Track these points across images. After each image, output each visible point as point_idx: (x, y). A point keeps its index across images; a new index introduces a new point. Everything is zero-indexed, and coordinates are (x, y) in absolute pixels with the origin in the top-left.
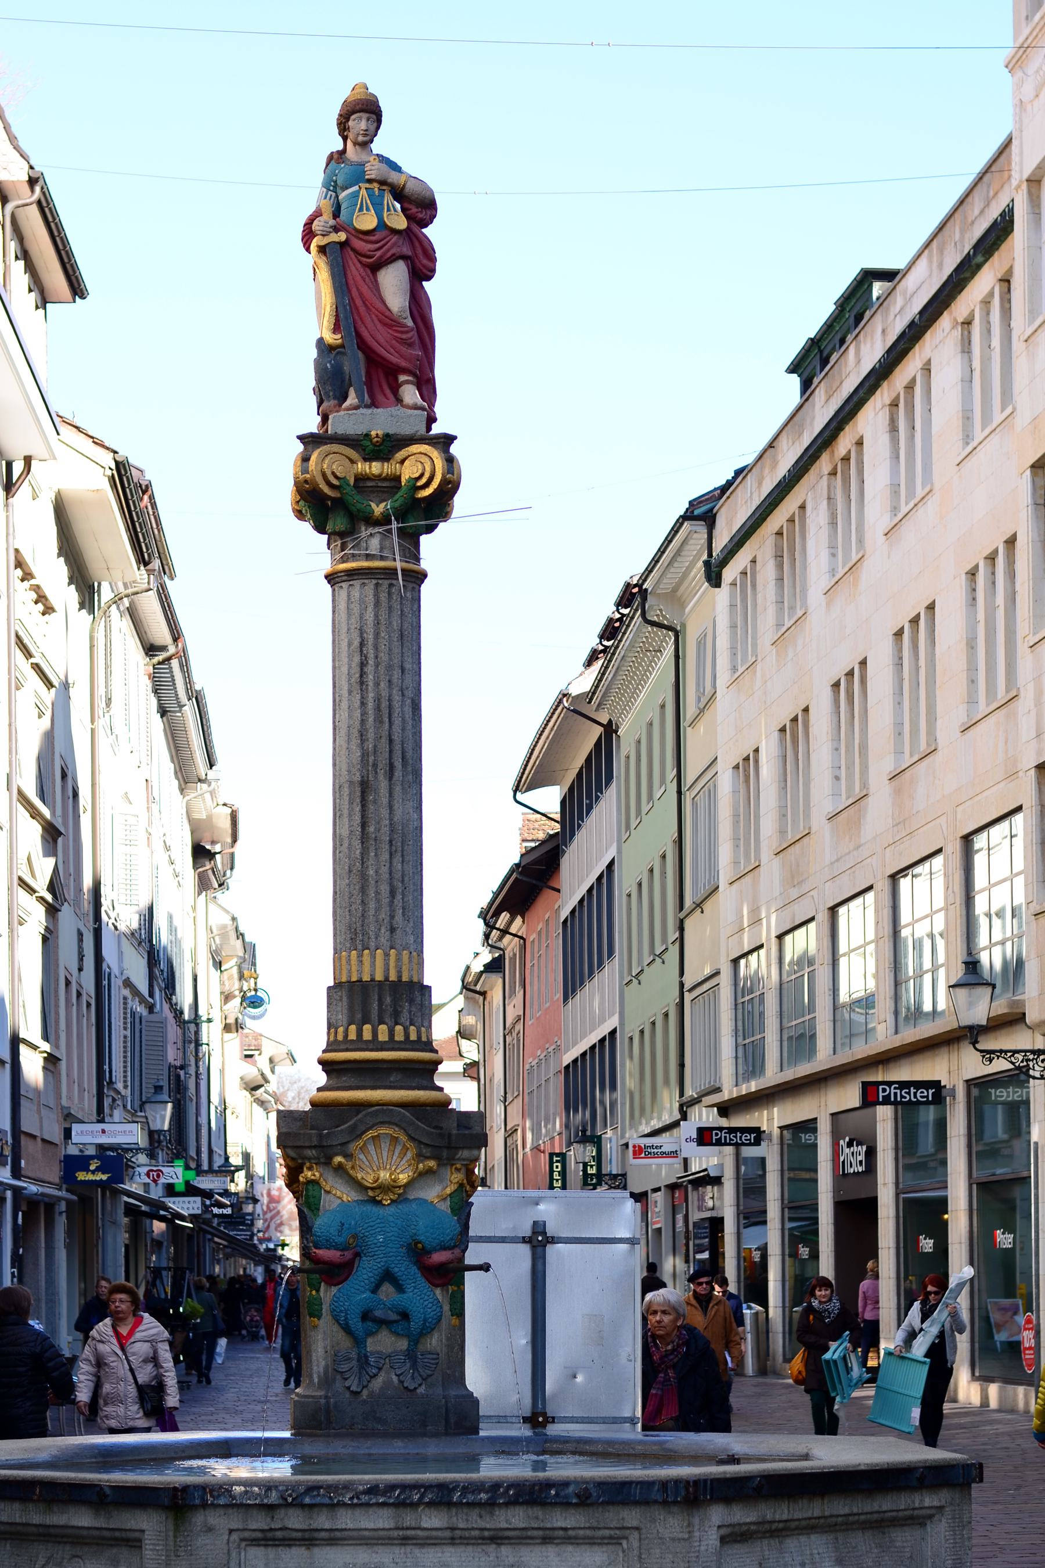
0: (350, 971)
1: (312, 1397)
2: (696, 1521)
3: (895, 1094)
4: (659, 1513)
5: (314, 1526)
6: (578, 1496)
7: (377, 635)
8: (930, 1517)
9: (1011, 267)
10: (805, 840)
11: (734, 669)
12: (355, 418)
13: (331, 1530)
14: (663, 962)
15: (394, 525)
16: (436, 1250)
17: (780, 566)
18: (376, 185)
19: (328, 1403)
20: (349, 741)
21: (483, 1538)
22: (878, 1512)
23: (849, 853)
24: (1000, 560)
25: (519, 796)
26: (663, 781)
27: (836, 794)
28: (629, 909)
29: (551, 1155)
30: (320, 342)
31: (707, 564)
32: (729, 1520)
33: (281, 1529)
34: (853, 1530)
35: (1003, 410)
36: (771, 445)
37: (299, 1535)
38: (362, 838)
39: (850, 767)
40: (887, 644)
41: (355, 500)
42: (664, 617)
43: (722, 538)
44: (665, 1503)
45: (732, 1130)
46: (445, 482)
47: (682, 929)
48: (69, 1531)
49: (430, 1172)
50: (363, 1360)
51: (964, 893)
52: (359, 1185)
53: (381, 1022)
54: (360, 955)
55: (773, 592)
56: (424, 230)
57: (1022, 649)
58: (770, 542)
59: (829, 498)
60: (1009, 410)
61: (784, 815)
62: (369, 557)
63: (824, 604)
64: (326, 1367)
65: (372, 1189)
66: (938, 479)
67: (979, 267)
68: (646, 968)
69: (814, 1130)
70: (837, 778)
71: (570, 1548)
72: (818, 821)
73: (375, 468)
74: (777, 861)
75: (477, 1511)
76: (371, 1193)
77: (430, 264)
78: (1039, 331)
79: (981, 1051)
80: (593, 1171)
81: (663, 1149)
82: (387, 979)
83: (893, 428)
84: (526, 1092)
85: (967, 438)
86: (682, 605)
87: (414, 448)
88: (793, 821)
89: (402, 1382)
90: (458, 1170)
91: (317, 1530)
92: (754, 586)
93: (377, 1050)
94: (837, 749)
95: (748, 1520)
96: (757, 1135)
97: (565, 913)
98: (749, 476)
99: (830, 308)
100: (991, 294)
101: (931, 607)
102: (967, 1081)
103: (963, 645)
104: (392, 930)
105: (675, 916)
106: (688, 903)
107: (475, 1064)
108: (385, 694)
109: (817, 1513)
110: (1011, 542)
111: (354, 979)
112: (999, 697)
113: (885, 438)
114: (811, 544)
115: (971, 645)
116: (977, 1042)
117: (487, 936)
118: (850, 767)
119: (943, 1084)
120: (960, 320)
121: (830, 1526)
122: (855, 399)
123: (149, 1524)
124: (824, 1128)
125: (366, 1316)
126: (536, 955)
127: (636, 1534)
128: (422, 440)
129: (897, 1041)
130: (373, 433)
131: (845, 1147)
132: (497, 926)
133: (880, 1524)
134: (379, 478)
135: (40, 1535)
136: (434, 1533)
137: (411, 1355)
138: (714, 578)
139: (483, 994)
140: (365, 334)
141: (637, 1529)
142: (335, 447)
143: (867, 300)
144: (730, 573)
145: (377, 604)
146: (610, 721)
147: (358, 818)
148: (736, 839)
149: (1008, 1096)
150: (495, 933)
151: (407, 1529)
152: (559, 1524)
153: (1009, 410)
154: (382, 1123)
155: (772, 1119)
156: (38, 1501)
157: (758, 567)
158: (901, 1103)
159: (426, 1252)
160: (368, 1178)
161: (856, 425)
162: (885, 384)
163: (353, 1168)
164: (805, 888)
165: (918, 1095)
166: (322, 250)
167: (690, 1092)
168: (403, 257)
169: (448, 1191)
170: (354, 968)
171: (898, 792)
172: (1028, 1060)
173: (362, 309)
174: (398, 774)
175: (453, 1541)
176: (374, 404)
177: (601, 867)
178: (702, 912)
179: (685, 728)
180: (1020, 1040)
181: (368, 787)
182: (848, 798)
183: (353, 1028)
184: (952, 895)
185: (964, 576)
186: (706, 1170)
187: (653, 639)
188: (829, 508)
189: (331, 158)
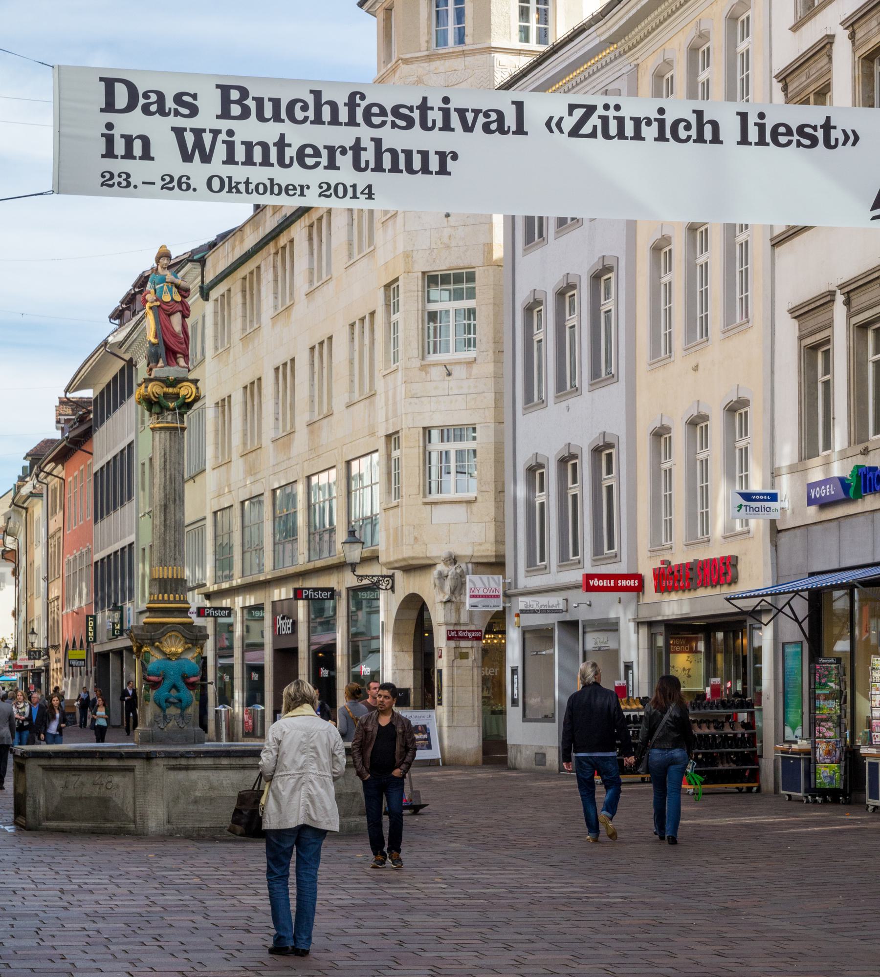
7: (170, 451)
10: (259, 451)
11: (216, 348)
17: (244, 297)
24: (367, 321)
27: (276, 428)
28: (143, 472)
29: (87, 616)
31: (201, 288)
35: (369, 247)
39: (284, 414)
40: (306, 354)
41: (164, 401)
43: (209, 277)
45: (216, 609)
46: (196, 396)
49: (189, 648)
50: (165, 717)
52: (164, 653)
57: (378, 375)
58: (239, 284)
59: (274, 267)
60: (372, 248)
62: (168, 422)
63: (271, 324)
66: (335, 274)
69: (263, 609)
70: (277, 419)
72: (266, 440)
73: (171, 390)
74: (241, 460)
80: (118, 627)
83: (310, 239)
84: (66, 575)
85: (350, 255)
87: (185, 384)
96: (229, 611)
97: (96, 468)
101: (330, 338)
103: (347, 362)
104: (175, 559)
110: (372, 314)
113: (305, 244)
115: (351, 362)
118: (284, 414)
123: (138, 764)
124: (268, 608)
125: (167, 701)
129: (310, 566)
132: (45, 470)
134: (171, 394)
137: (182, 715)
139: (26, 509)
144: (214, 294)
145: (170, 440)
146: (131, 359)
148: (216, 444)
150: (42, 475)
153: (372, 248)
155: (239, 602)
157: (232, 295)
158: (311, 599)
159: (188, 677)
160: (167, 650)
161: (290, 231)
162: (306, 215)
164: (259, 476)
171: (312, 432)
175: (231, 769)
177: (123, 444)
180: (375, 570)
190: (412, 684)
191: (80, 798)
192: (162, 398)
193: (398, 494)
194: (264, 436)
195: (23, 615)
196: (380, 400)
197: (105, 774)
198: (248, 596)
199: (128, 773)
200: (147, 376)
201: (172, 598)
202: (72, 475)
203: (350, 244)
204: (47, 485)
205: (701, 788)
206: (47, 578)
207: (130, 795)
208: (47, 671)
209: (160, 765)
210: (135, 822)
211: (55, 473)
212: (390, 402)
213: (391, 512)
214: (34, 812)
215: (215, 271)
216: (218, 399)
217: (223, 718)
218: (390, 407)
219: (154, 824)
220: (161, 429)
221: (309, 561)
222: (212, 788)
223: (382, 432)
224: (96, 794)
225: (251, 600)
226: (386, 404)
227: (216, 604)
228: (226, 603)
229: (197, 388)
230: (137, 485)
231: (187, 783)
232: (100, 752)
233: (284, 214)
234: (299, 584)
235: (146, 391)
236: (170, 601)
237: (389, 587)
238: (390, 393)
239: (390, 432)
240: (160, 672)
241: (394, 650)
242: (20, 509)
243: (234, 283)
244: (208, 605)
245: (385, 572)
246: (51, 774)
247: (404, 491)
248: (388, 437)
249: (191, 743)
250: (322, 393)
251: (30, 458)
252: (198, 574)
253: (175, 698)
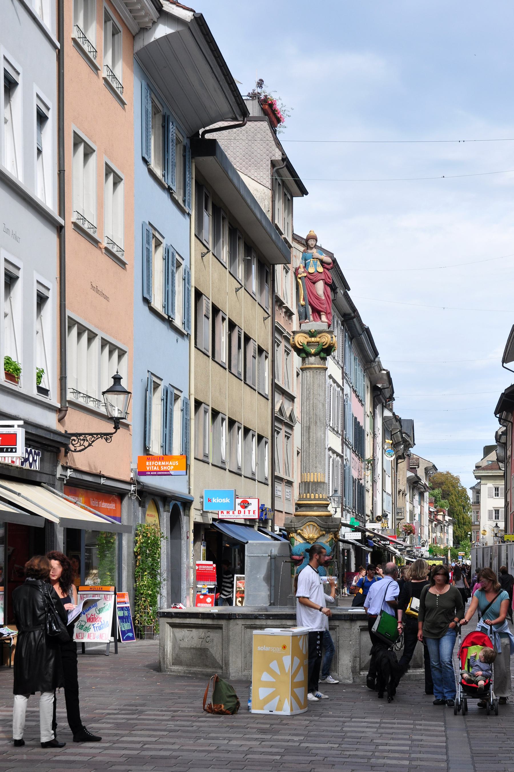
4: (343, 622)
25: (505, 365)
41: (308, 349)
52: (304, 539)
53: (312, 493)
73: (313, 339)
123: (223, 622)
127: (338, 628)
160: (306, 536)
205: (223, 679)
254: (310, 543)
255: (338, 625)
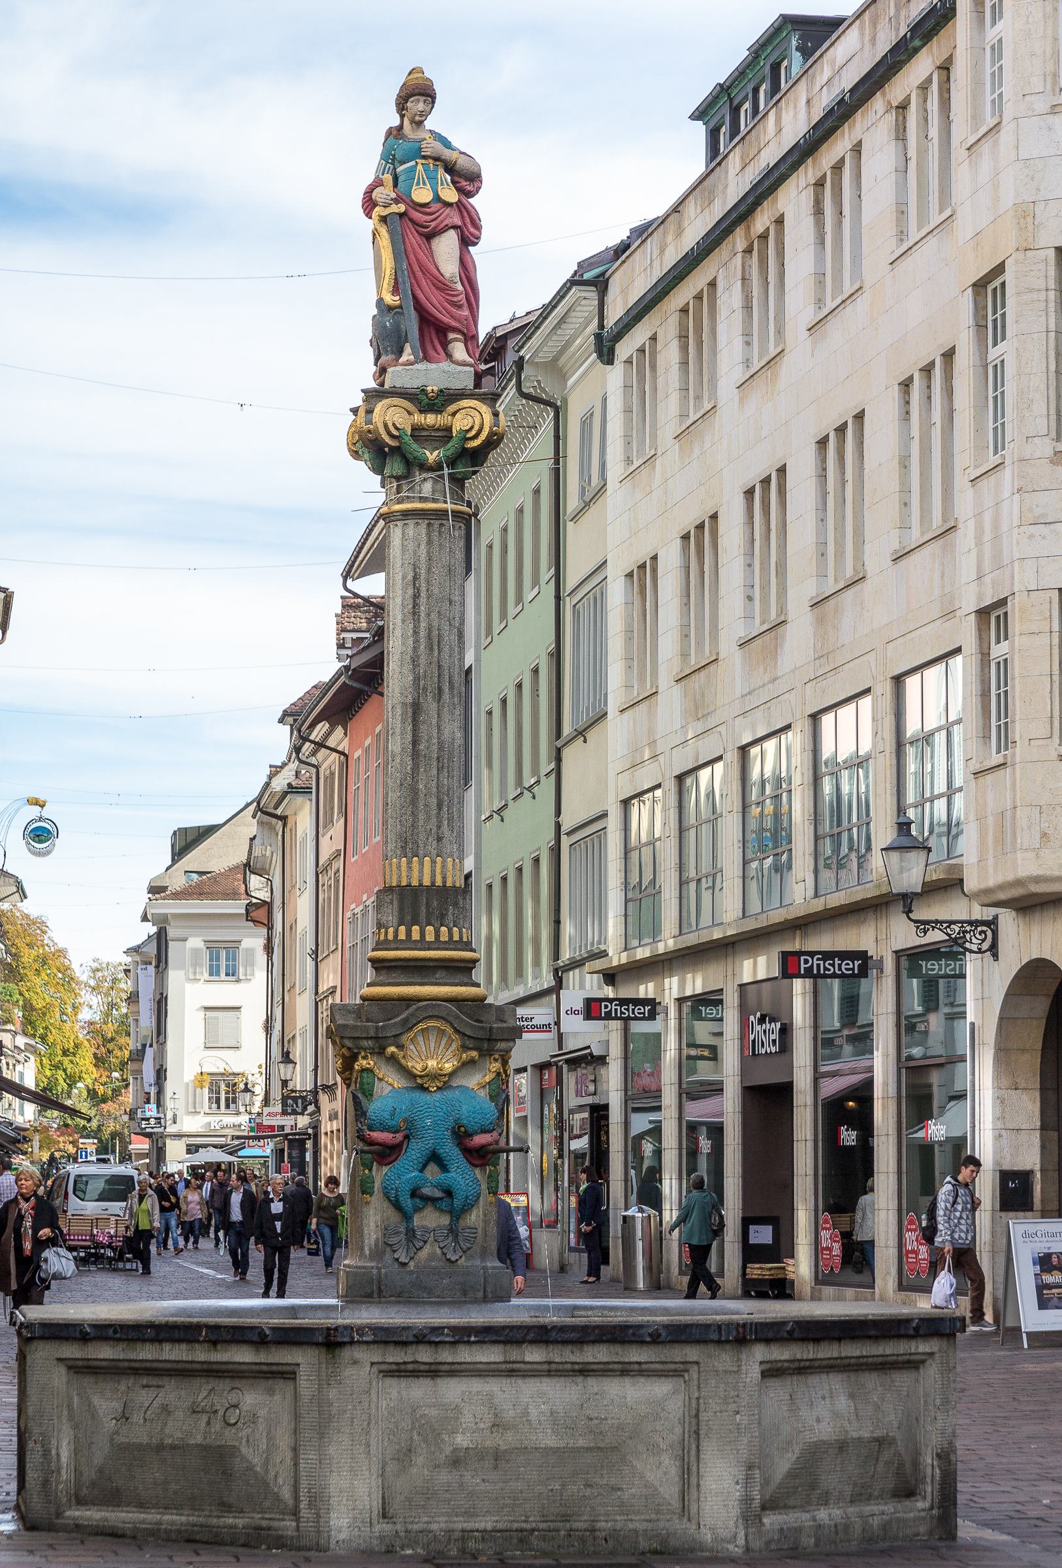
0: (400, 877)
1: (364, 1267)
2: (744, 1357)
3: (818, 965)
5: (440, 1359)
6: (650, 1335)
7: (429, 570)
8: (923, 1362)
9: (951, 55)
10: (712, 667)
11: (629, 461)
12: (411, 372)
13: (453, 1363)
14: (534, 797)
15: (446, 471)
16: (476, 1133)
17: (684, 348)
18: (431, 161)
19: (379, 1273)
20: (402, 666)
21: (573, 1371)
22: (883, 1356)
23: (764, 685)
24: (938, 372)
26: (536, 582)
27: (749, 617)
28: (490, 729)
30: (380, 302)
31: (598, 337)
32: (769, 1357)
33: (412, 1362)
34: (863, 1370)
36: (676, 209)
37: (426, 1367)
38: (413, 754)
39: (765, 587)
42: (543, 390)
43: (615, 312)
44: (719, 1342)
45: (623, 1002)
46: (492, 434)
47: (559, 760)
48: (231, 1367)
49: (472, 1062)
50: (411, 1234)
51: (894, 741)
52: (409, 1074)
54: (409, 863)
55: (677, 378)
56: (470, 200)
57: (961, 481)
58: (673, 320)
59: (743, 279)
60: (948, 213)
61: (686, 636)
62: (423, 499)
63: (736, 399)
64: (377, 1239)
65: (421, 1077)
66: (869, 279)
67: (916, 50)
68: (511, 803)
70: (750, 598)
71: (642, 1380)
72: (727, 646)
73: (431, 419)
74: (677, 689)
75: (570, 1347)
76: (419, 1081)
77: (476, 232)
78: (983, 141)
79: (915, 921)
81: (534, 1022)
82: (433, 884)
83: (818, 211)
84: (347, 945)
85: (902, 235)
86: (563, 377)
88: (697, 643)
89: (444, 1254)
90: (496, 1060)
91: (441, 1363)
92: (653, 367)
93: (425, 949)
94: (750, 565)
95: (783, 1358)
96: (652, 1008)
98: (649, 241)
99: (740, 55)
100: (929, 80)
101: (860, 417)
102: (896, 952)
103: (895, 463)
104: (439, 839)
105: (550, 743)
106: (567, 730)
107: (268, 905)
108: (435, 624)
109: (835, 1354)
110: (949, 355)
111: (404, 883)
112: (934, 527)
113: (809, 221)
114: (721, 328)
116: (910, 911)
117: (297, 749)
118: (765, 587)
119: (870, 954)
120: (895, 104)
121: (845, 1366)
122: (776, 174)
123: (304, 1359)
124: (731, 999)
125: (414, 1194)
126: (363, 777)
127: (695, 1368)
128: (471, 396)
129: (818, 905)
130: (429, 389)
131: (756, 1023)
132: (312, 737)
133: (885, 1366)
134: (432, 428)
135: (204, 1371)
136: (535, 1366)
137: (453, 1231)
138: (606, 353)
139: (283, 819)
140: (421, 296)
141: (697, 1363)
142: (397, 401)
143: (785, 49)
144: (625, 349)
145: (430, 542)
147: (409, 737)
148: (629, 659)
149: (940, 969)
150: (307, 747)
151: (514, 1362)
152: (635, 1359)
154: (431, 1017)
155: (671, 988)
156: (204, 1341)
157: (659, 348)
159: (469, 1135)
160: (417, 1066)
161: (776, 201)
162: (810, 160)
163: (404, 1057)
164: (712, 722)
165: (843, 967)
166: (384, 219)
167: (566, 955)
168: (455, 227)
169: (487, 1079)
170: (404, 874)
171: (820, 621)
172: (965, 932)
173: (419, 274)
174: (446, 696)
175: (549, 1373)
176: (427, 358)
178: (585, 741)
179: (565, 522)
180: (956, 909)
181: (418, 709)
182: (763, 623)
183: (402, 928)
184: (881, 742)
185: (896, 387)
186: (589, 1047)
187: (528, 413)
188: (743, 290)
189: (389, 133)
190: (1038, 1161)
191: (160, 1448)
192: (408, 439)
193: (1005, 740)
194: (723, 635)
195: (278, 1026)
196: (965, 538)
197: (223, 1385)
198: (689, 976)
199: (280, 1384)
200: (372, 384)
201: (430, 936)
202: (361, 745)
203: (902, 213)
204: (317, 767)
206: (316, 952)
207: (284, 1441)
208: (316, 1137)
209: (358, 1368)
210: (295, 1513)
211: (331, 742)
212: (987, 536)
213: (989, 778)
214: (46, 1483)
215: (626, 302)
216: (631, 564)
217: (639, 1234)
218: (987, 549)
219: (344, 1522)
220: (406, 514)
221: (816, 895)
222: (497, 1426)
223: (969, 603)
224: (199, 1439)
225: (696, 983)
226: (979, 543)
227: (626, 992)
228: (646, 990)
229: (496, 414)
230: (478, 756)
231: (433, 1412)
232: (208, 1327)
233: (763, 165)
234: (796, 945)
235: (369, 422)
236: (427, 941)
237: (985, 946)
238: (988, 517)
239: (988, 601)
240: (398, 1120)
241: (997, 1087)
242: (274, 820)
243: (663, 323)
244: (611, 996)
245: (979, 912)
246: (88, 1381)
247: (1018, 731)
248: (983, 614)
249: (475, 1301)
250: (844, 535)
251: (290, 720)
252: (592, 934)
253: (438, 1186)
254: (426, 1090)
255: (695, 1359)
